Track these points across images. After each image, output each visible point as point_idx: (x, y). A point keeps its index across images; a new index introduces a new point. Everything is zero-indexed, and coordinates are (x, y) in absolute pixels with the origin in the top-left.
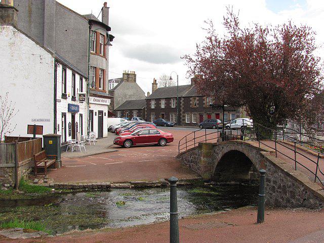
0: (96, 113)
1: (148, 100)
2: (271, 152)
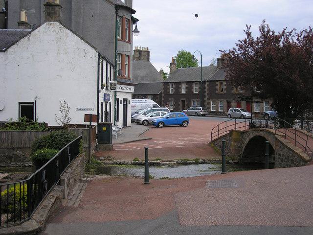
0: (121, 101)
1: (166, 84)
2: (283, 136)
